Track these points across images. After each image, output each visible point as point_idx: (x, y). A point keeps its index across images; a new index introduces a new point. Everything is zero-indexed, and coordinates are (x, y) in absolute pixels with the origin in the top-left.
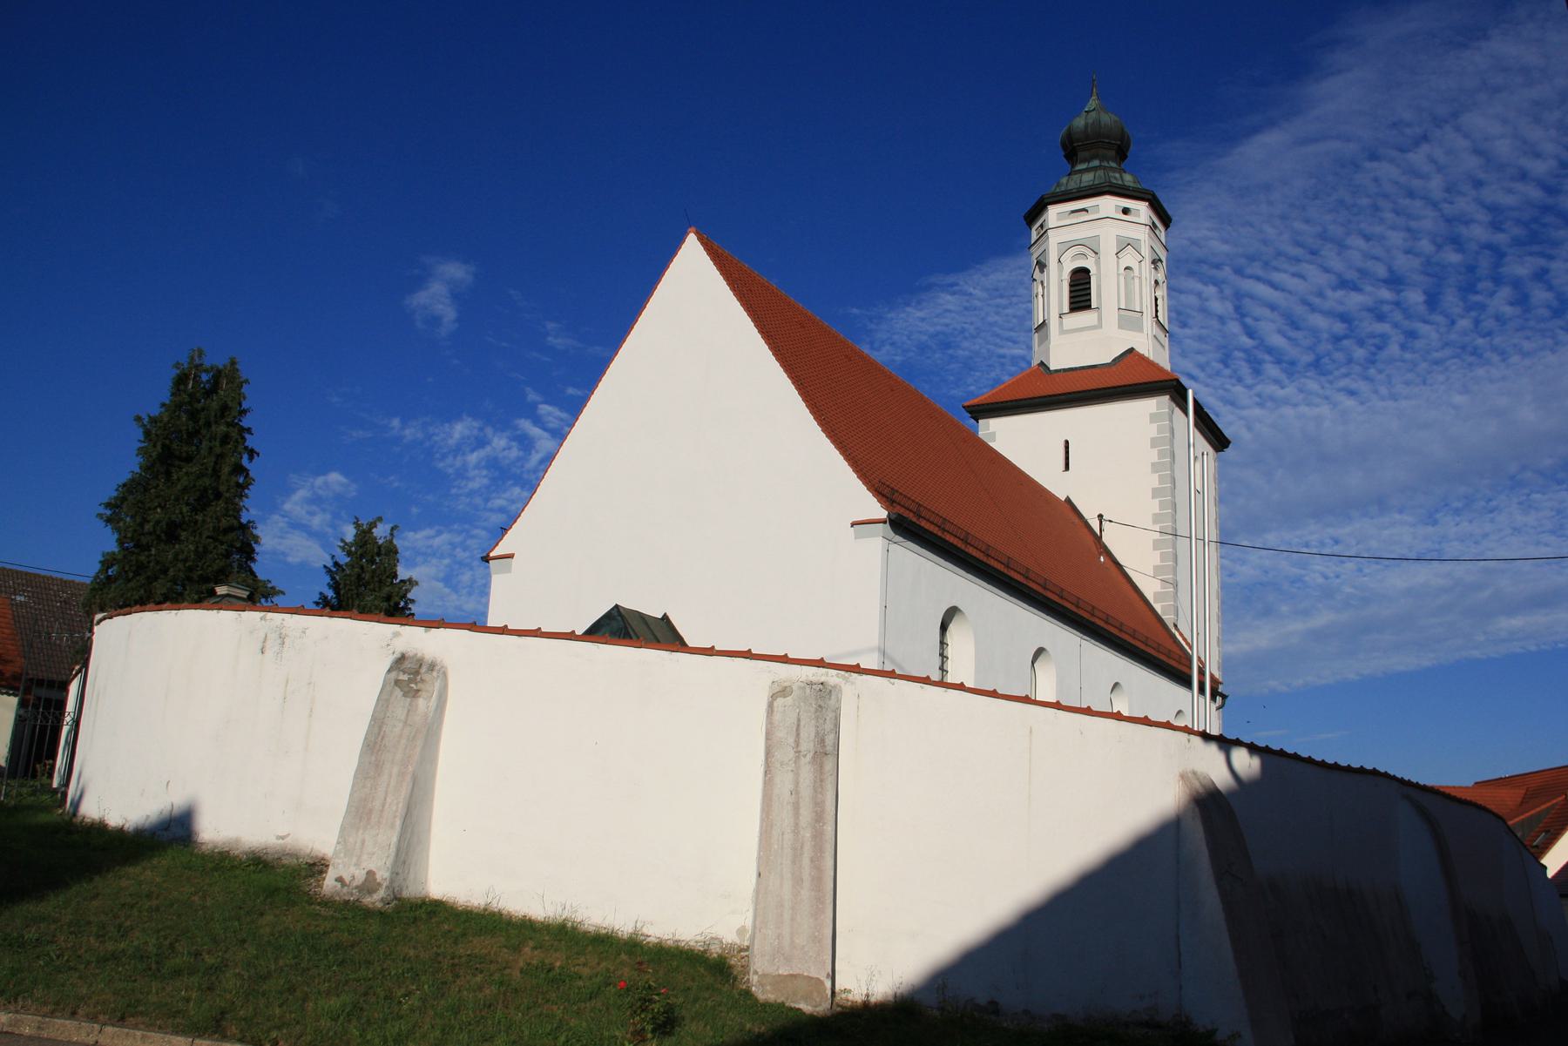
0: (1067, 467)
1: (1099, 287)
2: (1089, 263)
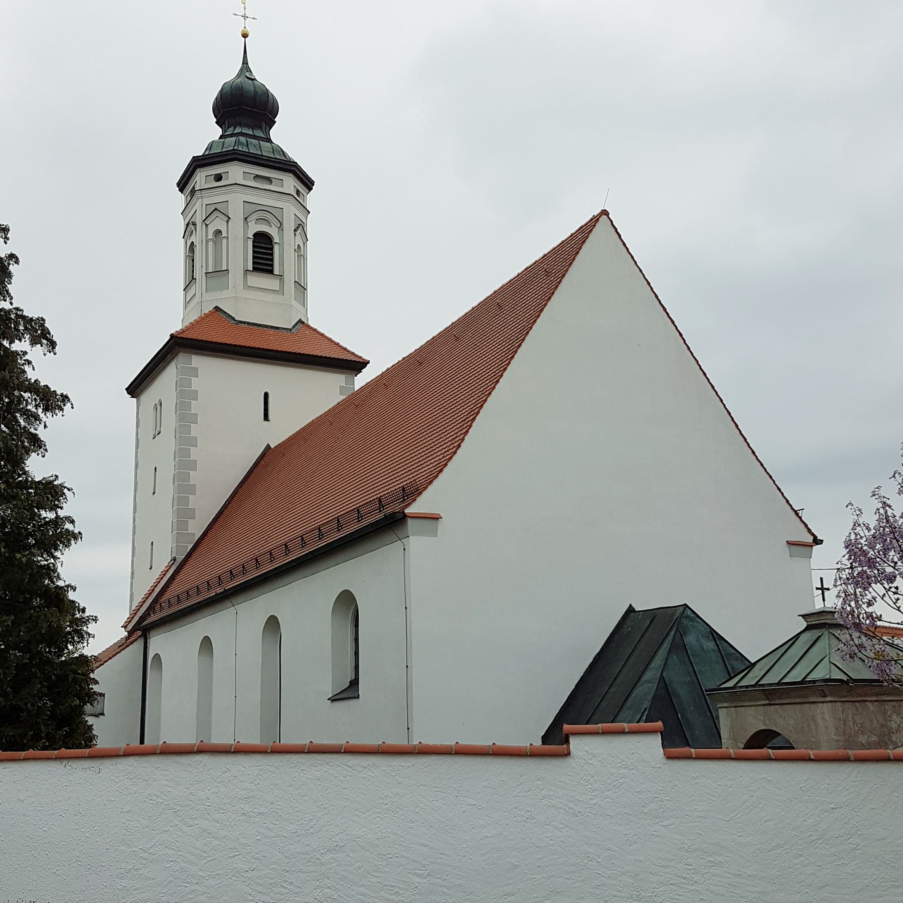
0: (266, 418)
1: (282, 256)
2: (273, 231)
